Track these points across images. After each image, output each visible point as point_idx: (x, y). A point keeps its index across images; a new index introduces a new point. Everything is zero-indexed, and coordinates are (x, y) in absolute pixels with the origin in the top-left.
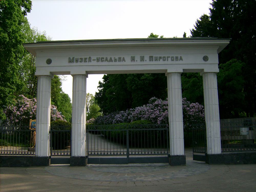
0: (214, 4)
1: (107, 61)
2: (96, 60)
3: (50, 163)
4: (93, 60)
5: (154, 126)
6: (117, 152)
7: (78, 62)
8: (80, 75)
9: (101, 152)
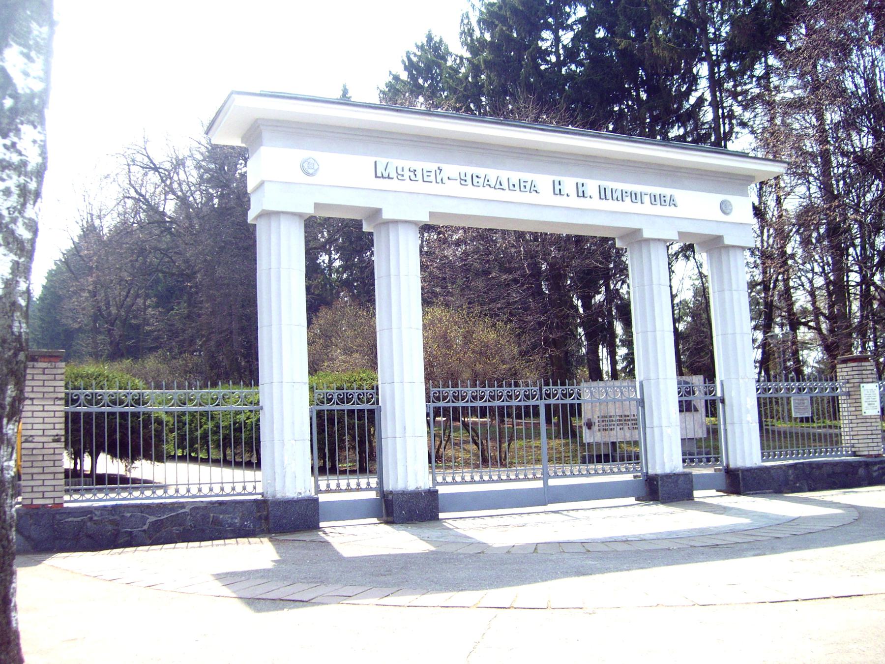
0: (490, 20)
5: (82, 397)
6: (177, 485)
8: (659, 240)
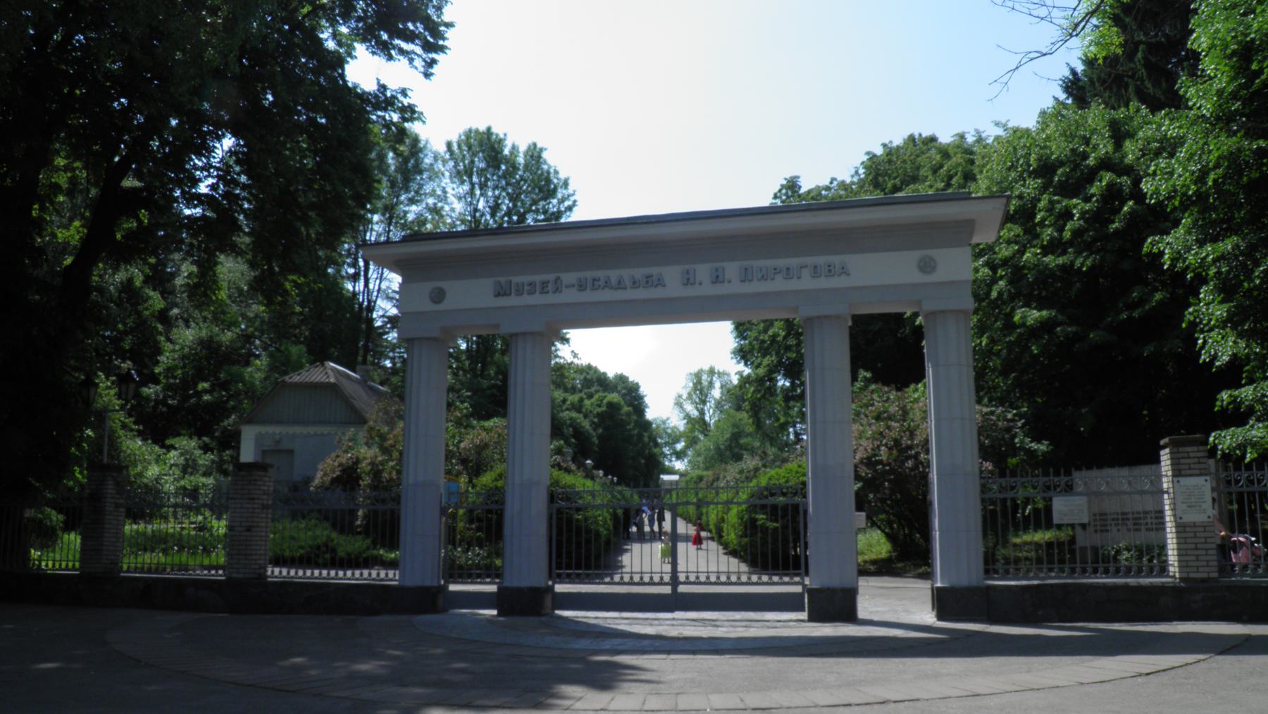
1: (608, 287)
2: (576, 286)
3: (780, 530)
4: (566, 287)
7: (522, 294)
9: (651, 573)
